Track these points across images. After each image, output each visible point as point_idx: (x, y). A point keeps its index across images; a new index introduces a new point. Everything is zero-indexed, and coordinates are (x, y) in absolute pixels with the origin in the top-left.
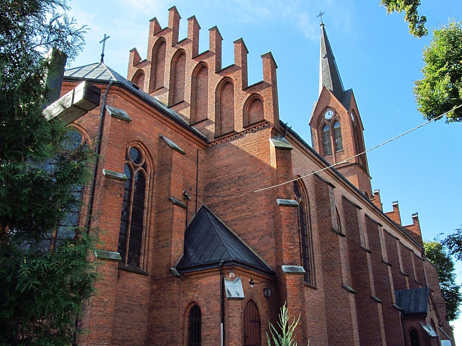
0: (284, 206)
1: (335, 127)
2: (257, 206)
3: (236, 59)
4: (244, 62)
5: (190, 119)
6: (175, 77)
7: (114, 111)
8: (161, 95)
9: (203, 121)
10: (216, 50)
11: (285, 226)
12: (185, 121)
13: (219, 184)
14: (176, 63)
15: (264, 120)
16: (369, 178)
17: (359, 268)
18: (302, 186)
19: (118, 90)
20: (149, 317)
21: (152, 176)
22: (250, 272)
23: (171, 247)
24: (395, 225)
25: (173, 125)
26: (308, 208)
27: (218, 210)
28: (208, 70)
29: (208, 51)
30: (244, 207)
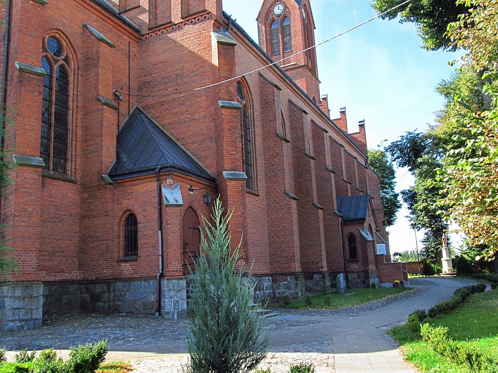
0: (226, 108)
5: (119, 5)
9: (134, 8)
12: (113, 8)
15: (205, 10)
16: (318, 82)
18: (246, 87)
20: (80, 227)
21: (76, 72)
22: (189, 178)
24: (341, 132)
25: (99, 12)
26: (252, 112)
27: (154, 112)
30: (183, 108)
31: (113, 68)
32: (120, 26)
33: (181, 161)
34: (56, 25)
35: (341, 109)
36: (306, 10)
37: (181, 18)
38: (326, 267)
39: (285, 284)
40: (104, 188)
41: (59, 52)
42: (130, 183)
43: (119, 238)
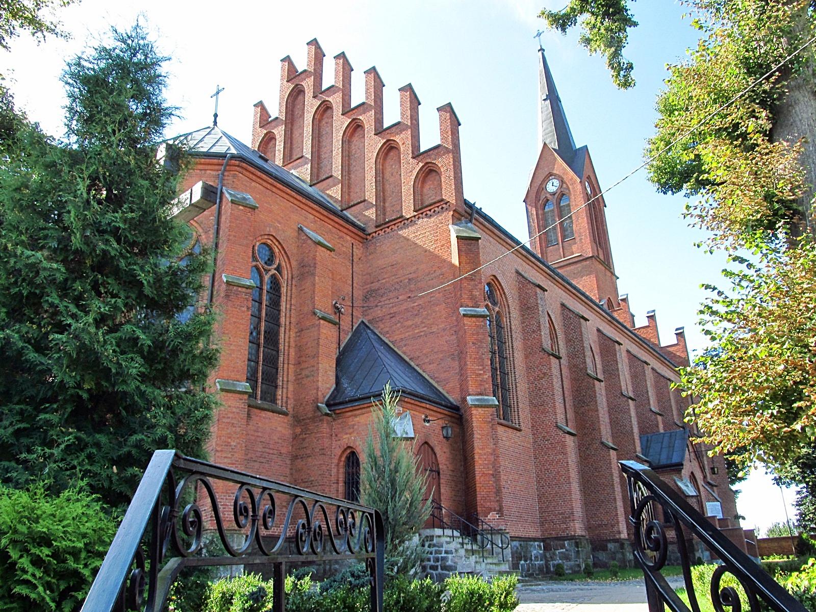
1: (562, 204)
2: (434, 318)
3: (402, 114)
4: (415, 118)
5: (341, 201)
6: (319, 141)
7: (234, 196)
8: (300, 168)
10: (375, 102)
12: (335, 204)
13: (383, 291)
14: (320, 121)
15: (442, 200)
16: (614, 278)
17: (584, 402)
19: (238, 166)
20: (291, 469)
22: (424, 405)
23: (318, 376)
25: (317, 211)
27: (382, 326)
29: (363, 104)
30: (418, 320)
33: (413, 385)
34: (268, 230)
35: (648, 313)
36: (591, 184)
37: (414, 211)
38: (625, 531)
39: (562, 553)
40: (320, 420)
41: (270, 261)
42: (350, 414)
43: (338, 483)
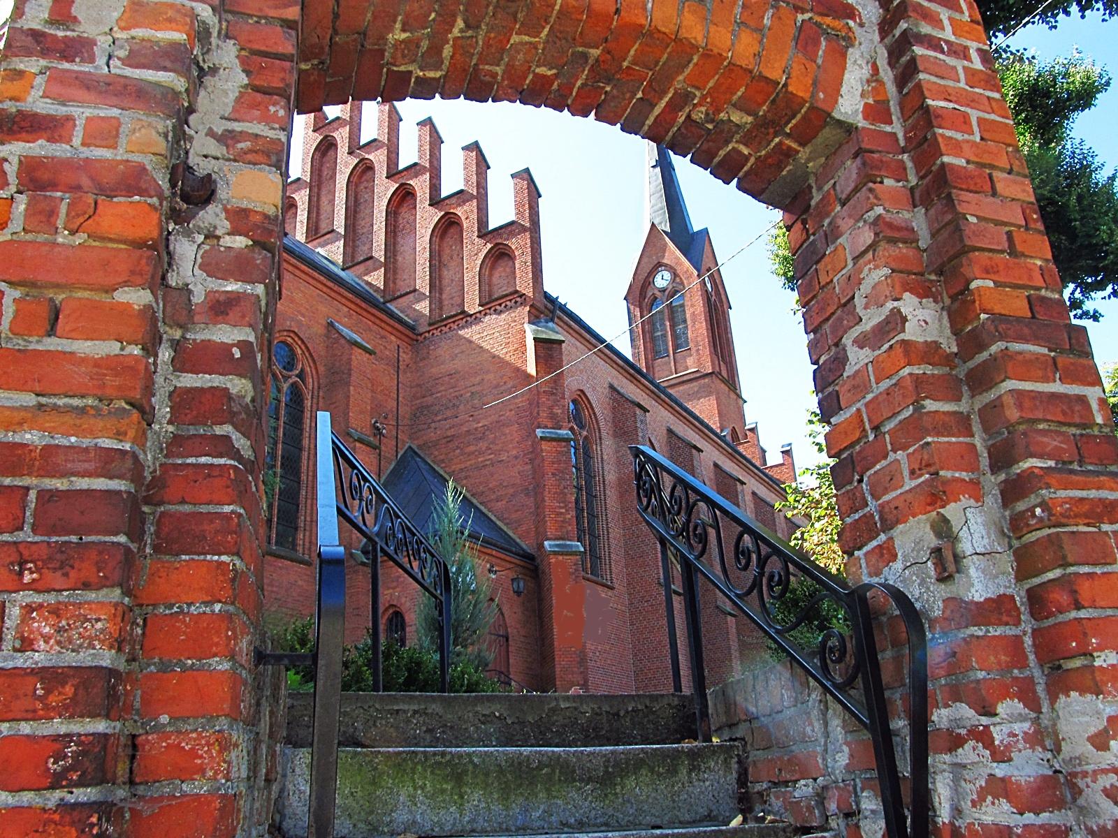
3: (467, 181)
5: (384, 291)
8: (329, 246)
9: (407, 294)
10: (431, 162)
11: (550, 475)
12: (375, 294)
15: (517, 292)
16: (742, 402)
21: (316, 393)
22: (489, 551)
25: (352, 302)
27: (436, 453)
28: (416, 200)
30: (483, 445)
31: (373, 385)
32: (385, 322)
